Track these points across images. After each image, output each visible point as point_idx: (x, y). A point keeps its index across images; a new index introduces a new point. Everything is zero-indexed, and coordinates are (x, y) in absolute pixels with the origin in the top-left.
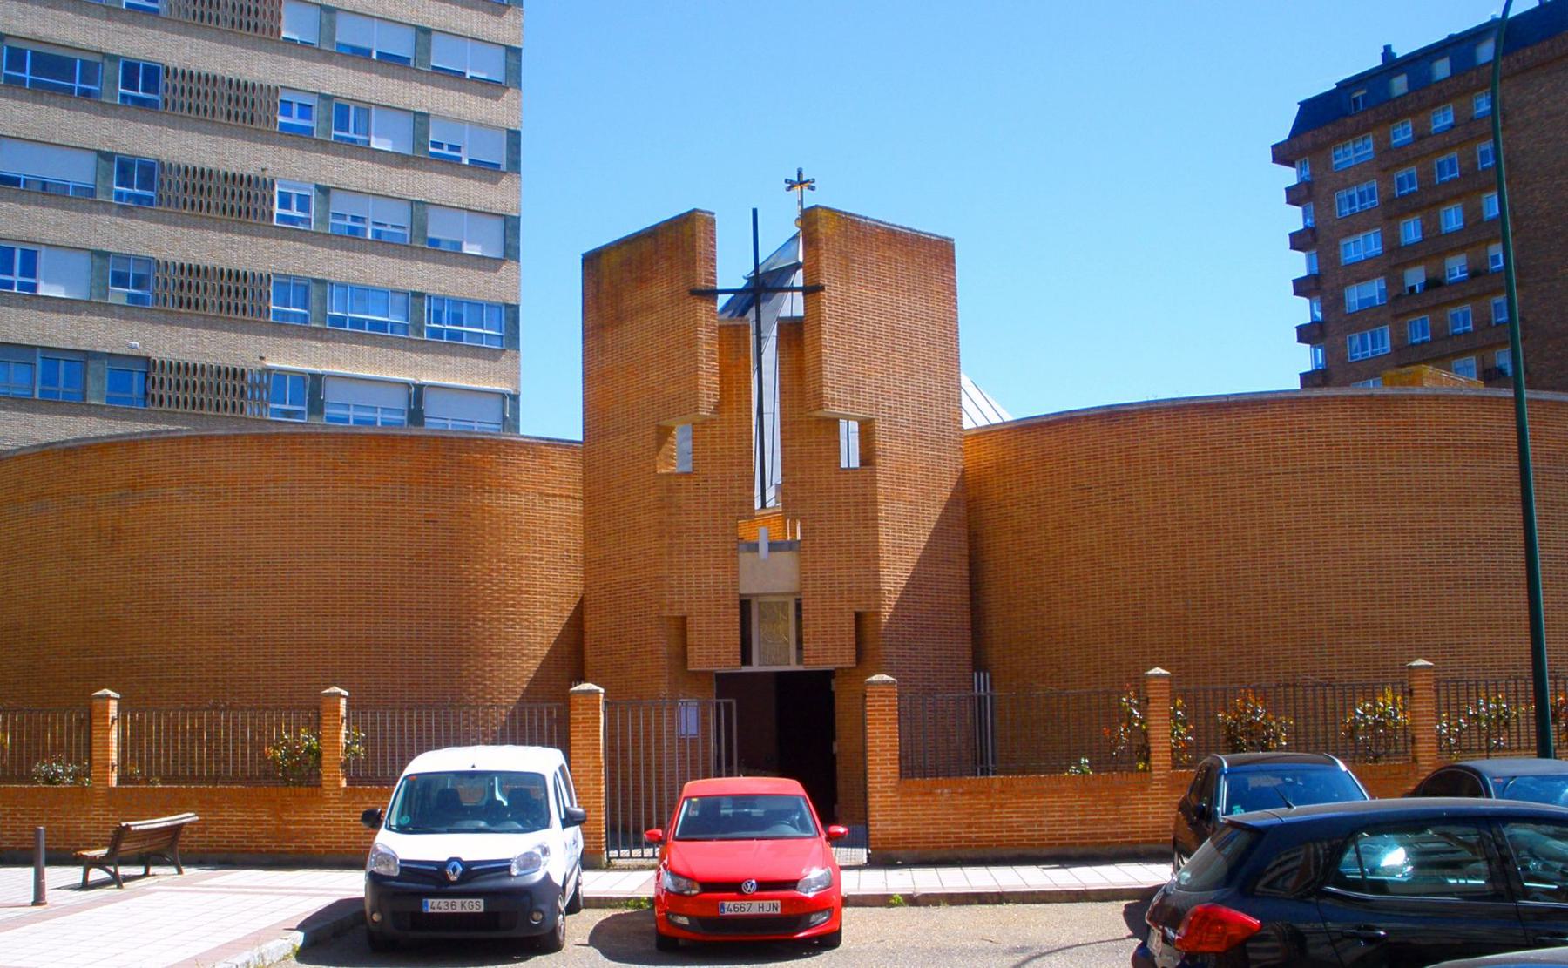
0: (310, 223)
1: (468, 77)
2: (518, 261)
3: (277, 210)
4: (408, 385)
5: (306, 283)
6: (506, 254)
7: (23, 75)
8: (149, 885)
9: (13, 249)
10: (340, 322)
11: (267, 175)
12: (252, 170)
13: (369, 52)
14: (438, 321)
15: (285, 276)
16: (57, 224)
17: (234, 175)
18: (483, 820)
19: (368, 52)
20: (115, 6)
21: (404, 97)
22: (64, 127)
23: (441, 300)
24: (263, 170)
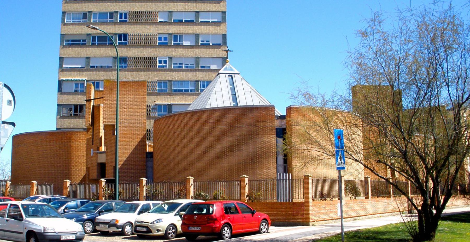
1: (211, 22)
3: (158, 64)
13: (183, 20)
23: (204, 82)
24: (154, 55)
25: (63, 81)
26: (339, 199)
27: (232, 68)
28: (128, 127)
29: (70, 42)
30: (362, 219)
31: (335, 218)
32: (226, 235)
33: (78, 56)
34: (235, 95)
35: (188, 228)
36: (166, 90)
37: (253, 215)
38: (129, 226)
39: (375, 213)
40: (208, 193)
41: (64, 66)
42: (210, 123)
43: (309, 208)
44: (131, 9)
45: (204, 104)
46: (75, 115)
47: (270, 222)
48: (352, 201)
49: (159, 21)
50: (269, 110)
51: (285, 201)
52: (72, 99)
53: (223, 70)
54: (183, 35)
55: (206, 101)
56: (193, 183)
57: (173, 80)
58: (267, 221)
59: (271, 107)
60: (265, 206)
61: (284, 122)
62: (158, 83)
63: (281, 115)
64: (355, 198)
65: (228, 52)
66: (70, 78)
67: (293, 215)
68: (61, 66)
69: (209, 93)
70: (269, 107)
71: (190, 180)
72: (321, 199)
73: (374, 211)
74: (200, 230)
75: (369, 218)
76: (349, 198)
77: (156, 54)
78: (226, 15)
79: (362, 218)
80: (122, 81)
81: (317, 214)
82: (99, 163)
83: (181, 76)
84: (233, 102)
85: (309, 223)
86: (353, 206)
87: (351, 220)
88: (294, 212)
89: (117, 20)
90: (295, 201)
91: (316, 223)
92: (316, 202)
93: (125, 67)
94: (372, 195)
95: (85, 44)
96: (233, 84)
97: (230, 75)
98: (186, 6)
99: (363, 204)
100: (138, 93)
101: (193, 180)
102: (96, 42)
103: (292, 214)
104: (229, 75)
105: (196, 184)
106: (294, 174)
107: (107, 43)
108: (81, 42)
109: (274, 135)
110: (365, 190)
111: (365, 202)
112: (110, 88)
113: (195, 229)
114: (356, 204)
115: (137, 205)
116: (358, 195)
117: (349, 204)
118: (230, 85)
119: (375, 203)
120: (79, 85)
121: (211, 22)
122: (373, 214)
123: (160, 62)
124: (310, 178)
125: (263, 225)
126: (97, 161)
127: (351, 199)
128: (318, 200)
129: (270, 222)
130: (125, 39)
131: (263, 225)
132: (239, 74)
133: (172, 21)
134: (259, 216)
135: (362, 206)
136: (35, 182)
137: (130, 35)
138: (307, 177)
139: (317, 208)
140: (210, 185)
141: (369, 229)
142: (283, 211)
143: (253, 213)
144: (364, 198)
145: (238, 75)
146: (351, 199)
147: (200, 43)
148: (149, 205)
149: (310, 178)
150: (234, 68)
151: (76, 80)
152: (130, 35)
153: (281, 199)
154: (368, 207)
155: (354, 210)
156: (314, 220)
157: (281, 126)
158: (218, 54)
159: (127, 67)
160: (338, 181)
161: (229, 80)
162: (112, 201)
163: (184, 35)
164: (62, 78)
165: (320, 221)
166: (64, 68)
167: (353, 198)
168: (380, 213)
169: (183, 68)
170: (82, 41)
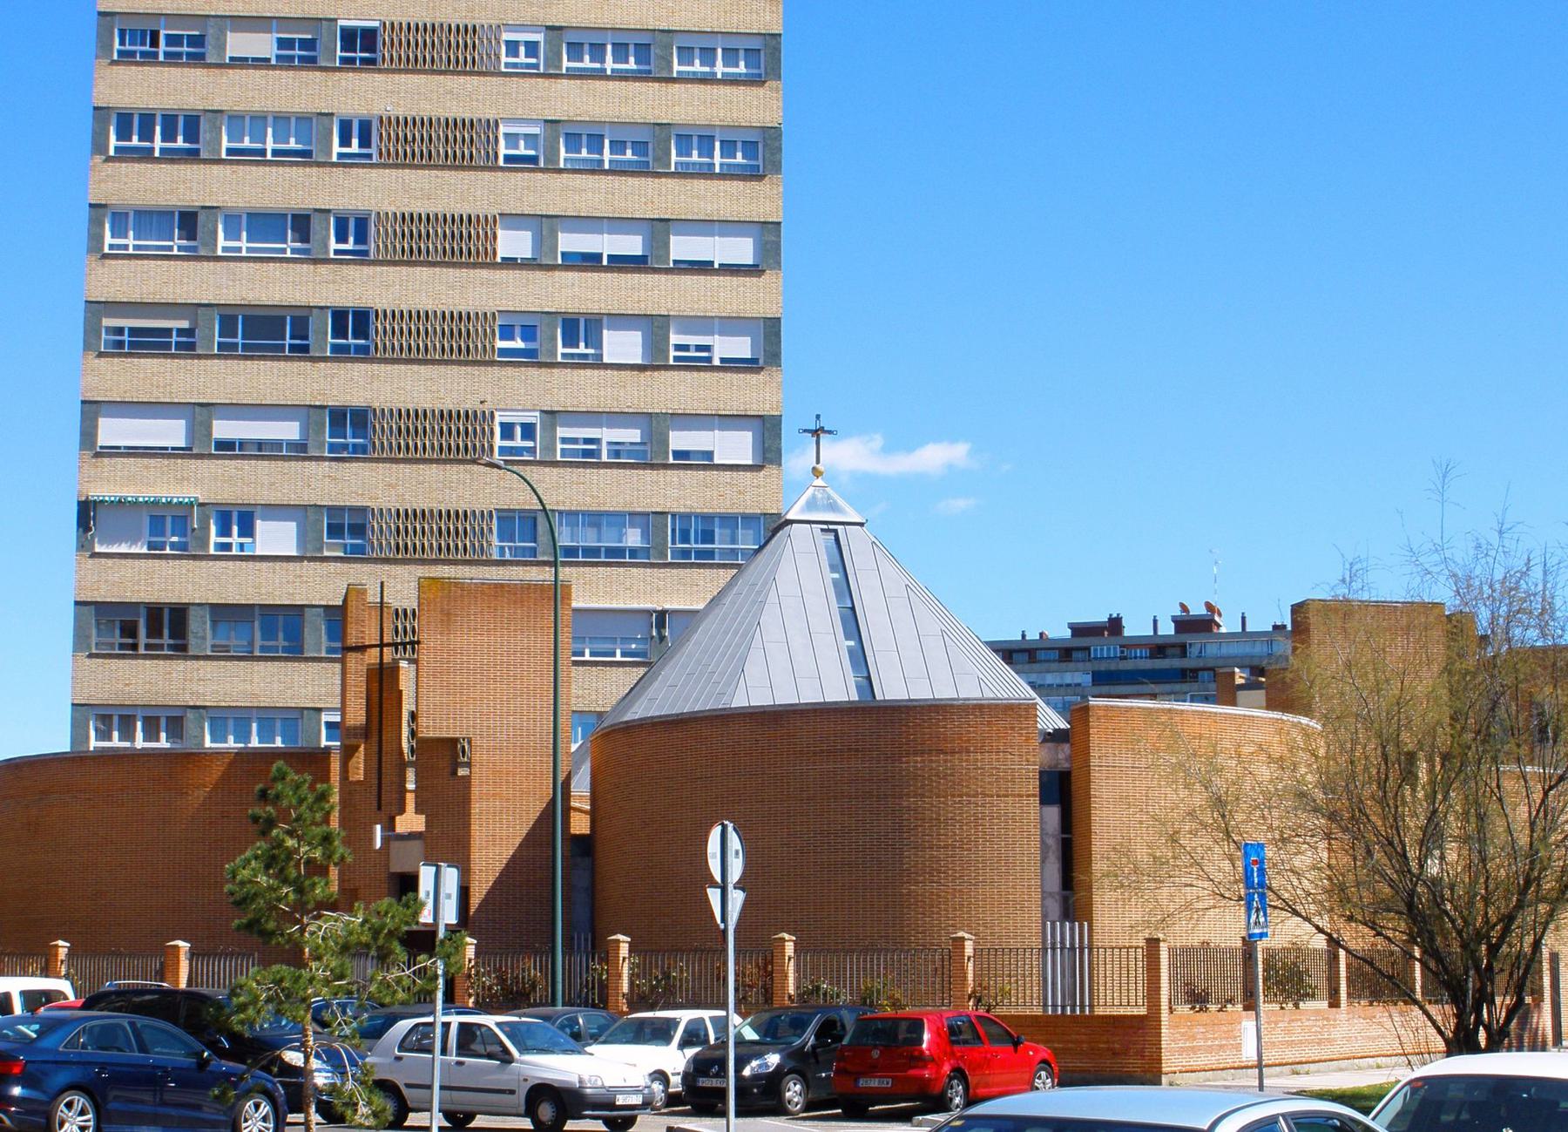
0: (535, 452)
1: (716, 266)
2: (780, 465)
3: (498, 442)
4: (649, 612)
5: (533, 515)
6: (764, 459)
7: (288, 336)
8: (212, 1114)
9: (231, 512)
10: (571, 551)
11: (487, 408)
12: (470, 404)
13: (600, 255)
14: (686, 539)
15: (509, 510)
16: (273, 484)
17: (450, 412)
18: (17, 1085)
19: (598, 257)
20: (323, 257)
21: (639, 301)
22: (275, 386)
23: (686, 517)
24: (482, 402)
25: (97, 504)
26: (1246, 1008)
27: (835, 502)
28: (508, 748)
29: (126, 338)
30: (1318, 1071)
31: (1236, 1065)
32: (957, 1100)
33: (162, 400)
34: (853, 608)
35: (856, 1080)
36: (534, 552)
37: (1016, 1050)
38: (658, 1082)
39: (1359, 1055)
40: (845, 987)
41: (104, 439)
42: (822, 751)
43: (1159, 1034)
44: (386, 202)
45: (739, 646)
46: (148, 647)
47: (1056, 1070)
48: (1284, 1014)
49: (503, 259)
50: (1020, 716)
51: (1087, 1013)
52: (140, 580)
53: (802, 511)
54: (601, 320)
55: (744, 636)
56: (792, 955)
57: (561, 508)
58: (1050, 1066)
59: (1024, 704)
60: (1028, 1026)
61: (1063, 750)
62: (498, 518)
63: (1055, 730)
64: (1297, 1006)
65: (818, 436)
66: (129, 493)
67: (1115, 1054)
68: (88, 436)
69: (754, 602)
70: (1020, 704)
71: (787, 944)
72: (1192, 1009)
73: (1357, 1047)
74: (890, 1085)
75: (1341, 1070)
76: (1276, 1007)
77: (489, 398)
78: (779, 236)
79: (1315, 1069)
80: (483, 584)
81: (1182, 1050)
82: (393, 874)
83: (595, 493)
84: (847, 638)
85: (1160, 1077)
86: (1288, 1032)
87: (1282, 1072)
88: (1117, 1046)
89: (326, 246)
90: (1099, 1011)
91: (1178, 1078)
92: (1180, 1017)
93: (364, 449)
94: (1349, 995)
95: (192, 346)
96: (840, 564)
97: (830, 528)
98: (613, 194)
99: (1320, 1023)
100: (542, 628)
101: (792, 944)
102: (239, 340)
103: (1108, 1049)
104: (825, 527)
105: (805, 959)
106: (1097, 925)
107: (284, 345)
108: (174, 339)
109: (1034, 795)
110: (1329, 979)
111: (1328, 1019)
112: (442, 610)
113: (876, 1085)
114: (1299, 1024)
115: (674, 1023)
116: (1307, 995)
117: (1276, 1023)
118: (833, 568)
119: (1359, 1024)
120: (169, 521)
121: (716, 266)
122: (1354, 1058)
123: (507, 430)
124: (1162, 944)
125: (1040, 1078)
126: (387, 866)
127: (1282, 1008)
128: (1184, 1009)
129: (1056, 1070)
130: (361, 331)
131: (1040, 1078)
132: (862, 525)
133: (556, 259)
134: (1031, 1053)
135: (1318, 1029)
136: (184, 945)
137: (381, 315)
138: (1153, 944)
139: (1183, 1034)
140: (851, 962)
141: (1331, 1091)
142: (1082, 1042)
143: (1016, 1043)
144: (1325, 1004)
145: (858, 527)
146: (1282, 1008)
147: (672, 353)
148: (702, 1020)
149: (1163, 947)
150: (841, 502)
151: (156, 503)
152: (381, 315)
153: (1082, 1006)
154: (1336, 1034)
155: (1291, 1044)
156: (1173, 1069)
157: (1053, 763)
158: (745, 403)
159: (370, 448)
160: (1245, 953)
161: (826, 547)
162: (577, 1012)
163: (605, 318)
164: (97, 492)
165: (1192, 1072)
166: (101, 447)
167: (1290, 1005)
168: (1378, 1056)
169: (600, 457)
170: (177, 336)
